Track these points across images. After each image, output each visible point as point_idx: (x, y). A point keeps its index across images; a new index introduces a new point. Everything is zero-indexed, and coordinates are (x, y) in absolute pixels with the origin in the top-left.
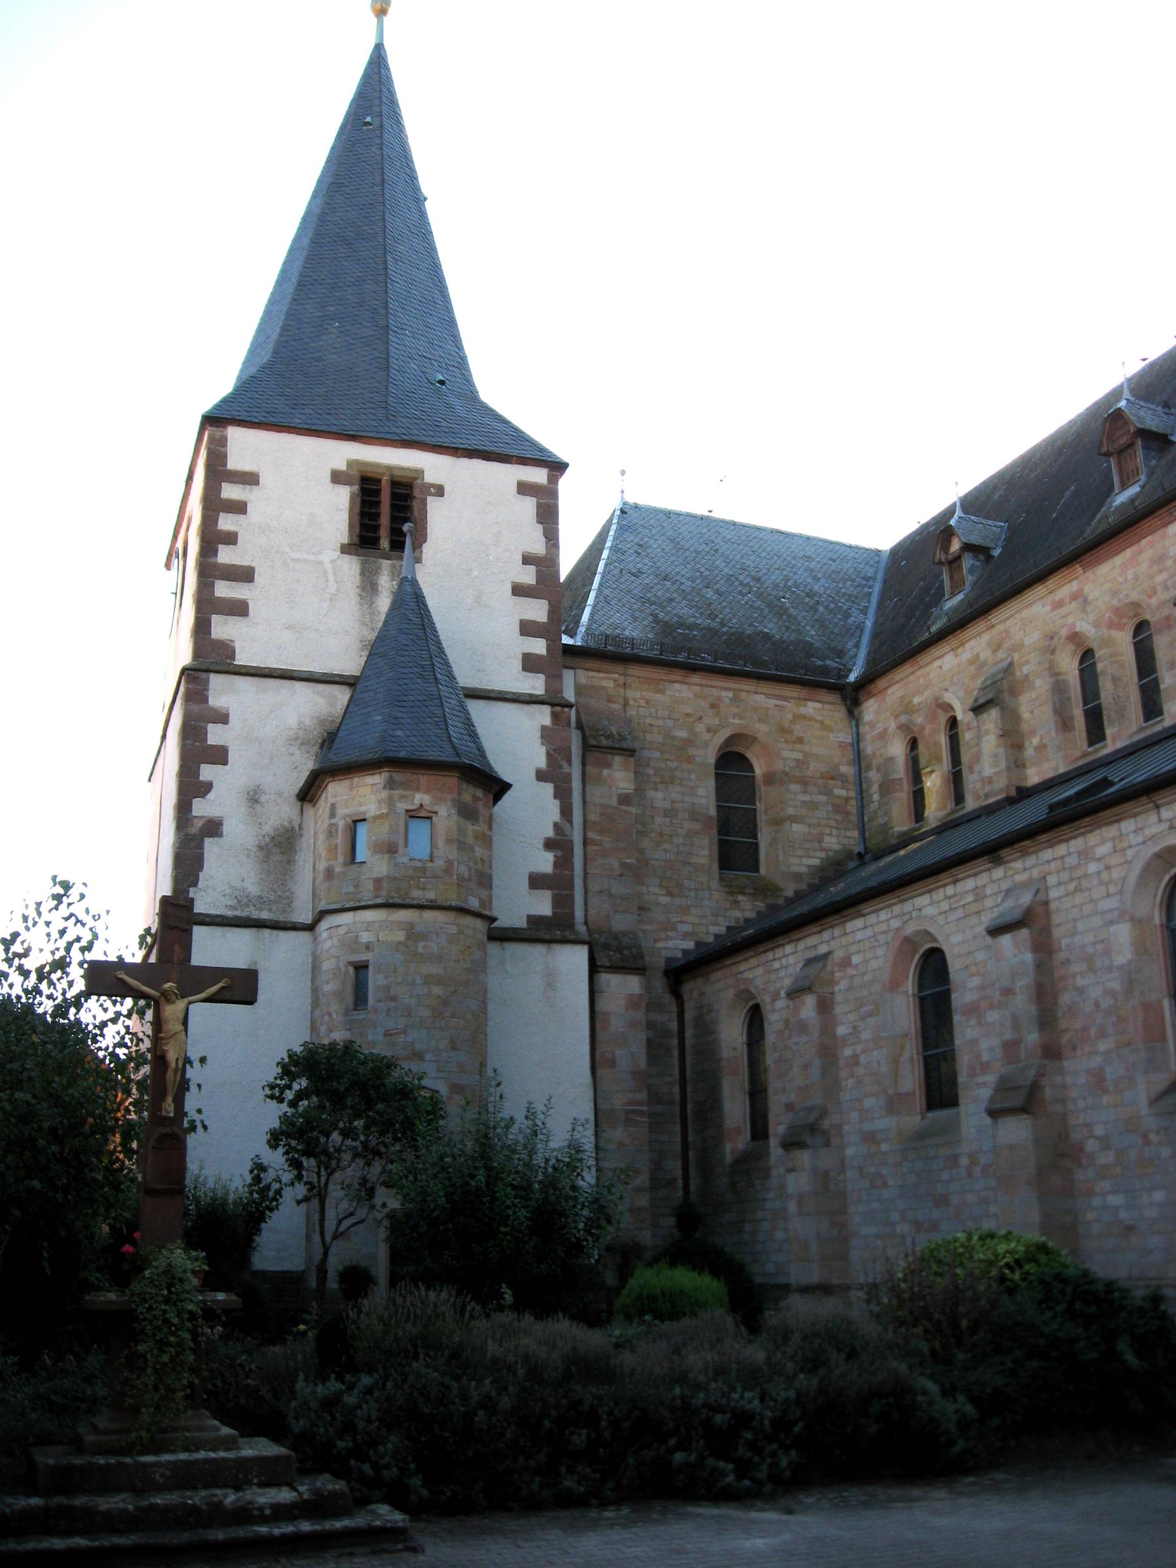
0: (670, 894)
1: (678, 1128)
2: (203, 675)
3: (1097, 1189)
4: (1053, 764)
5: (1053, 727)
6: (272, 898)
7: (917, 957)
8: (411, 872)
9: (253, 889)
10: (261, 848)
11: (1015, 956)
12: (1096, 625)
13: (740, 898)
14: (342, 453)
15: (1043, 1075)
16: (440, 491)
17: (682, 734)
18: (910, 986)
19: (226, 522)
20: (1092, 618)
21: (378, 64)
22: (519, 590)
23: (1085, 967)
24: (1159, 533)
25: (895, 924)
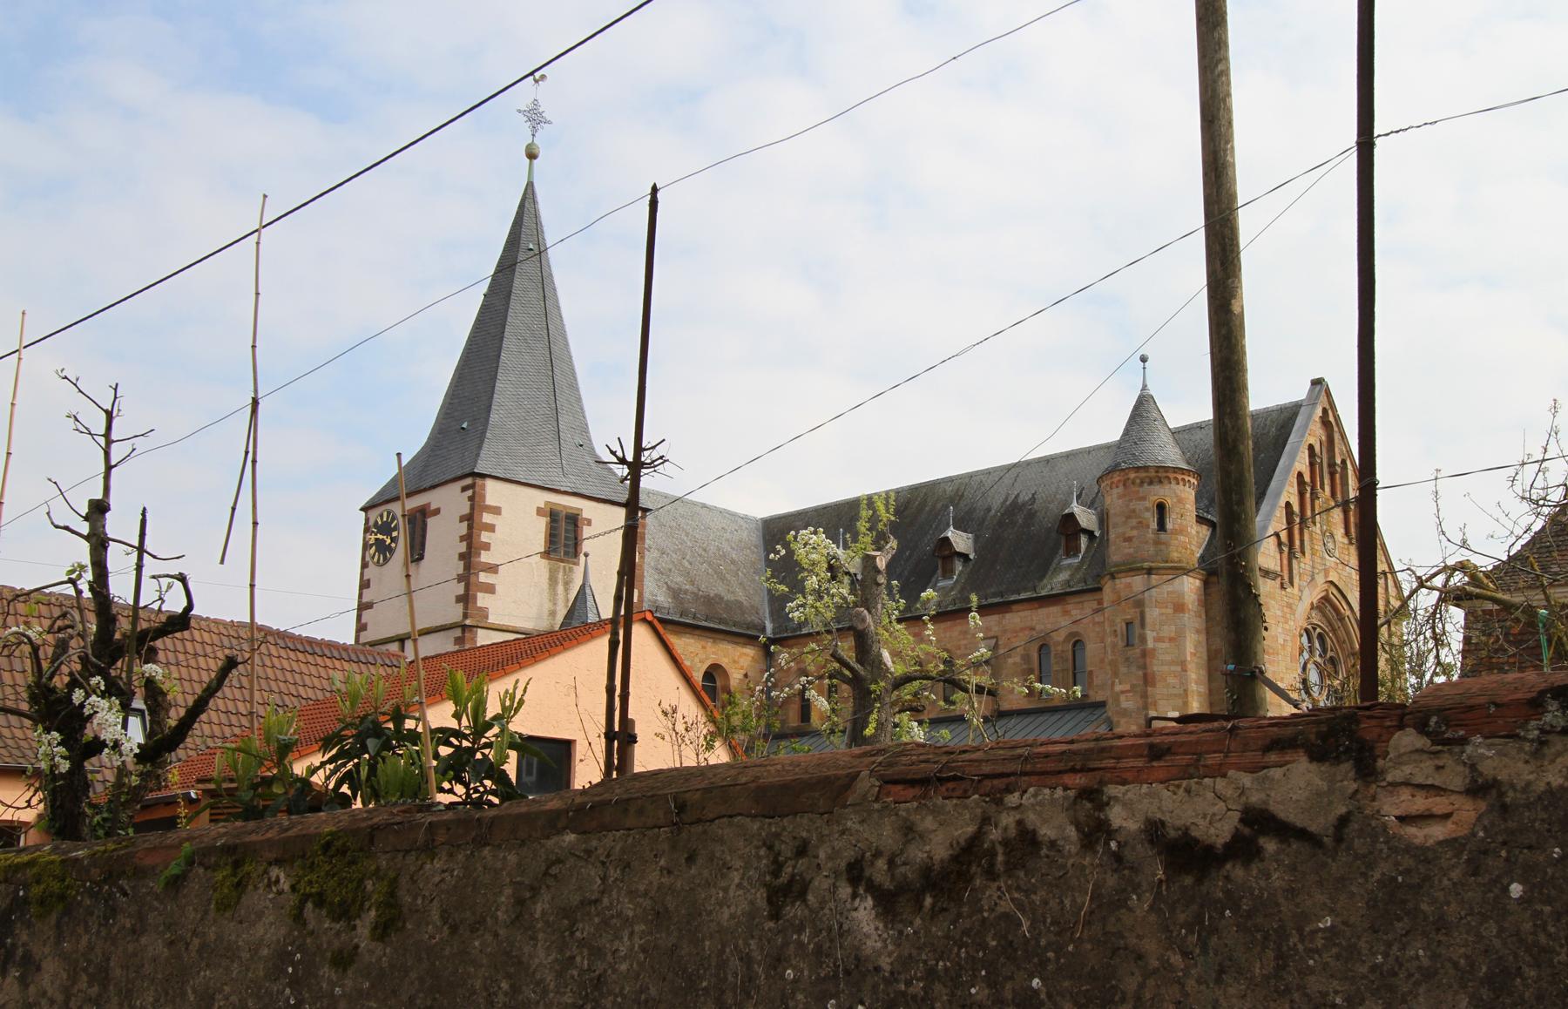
14: (542, 498)
16: (589, 522)
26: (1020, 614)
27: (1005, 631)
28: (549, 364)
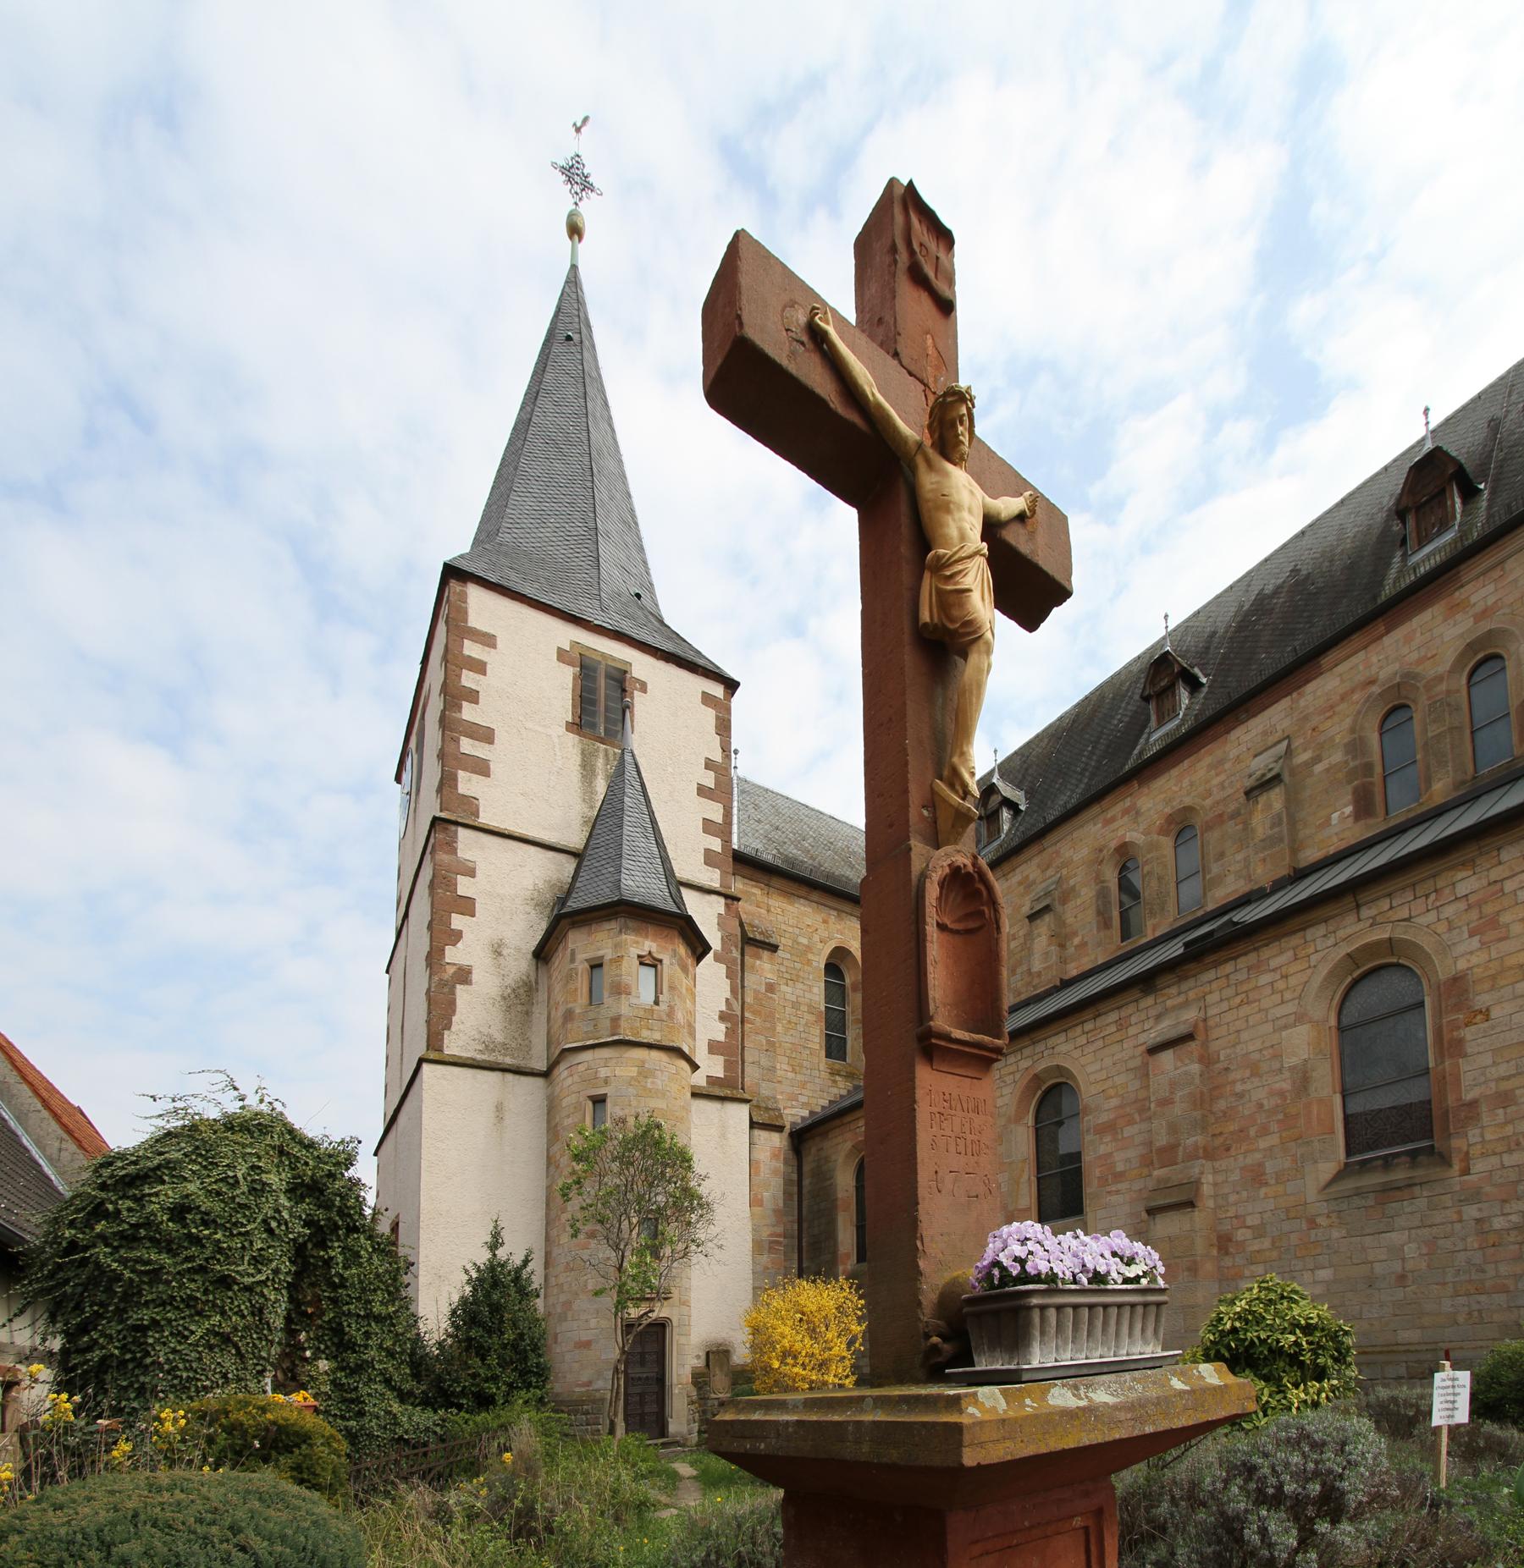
0: (794, 1071)
1: (796, 1256)
2: (453, 828)
3: (1247, 1273)
4: (1093, 957)
5: (1095, 926)
6: (514, 1045)
7: (1040, 1092)
8: (641, 1014)
9: (499, 1037)
10: (504, 998)
11: (1176, 1069)
12: (1146, 833)
13: (838, 1078)
15: (1202, 1173)
17: (804, 941)
18: (1030, 1119)
19: (468, 679)
20: (1141, 828)
21: (573, 280)
22: (702, 791)
23: (1248, 1073)
24: (1222, 739)
25: (1024, 1064)
26: (1340, 669)
27: (1306, 718)
28: (588, 473)
